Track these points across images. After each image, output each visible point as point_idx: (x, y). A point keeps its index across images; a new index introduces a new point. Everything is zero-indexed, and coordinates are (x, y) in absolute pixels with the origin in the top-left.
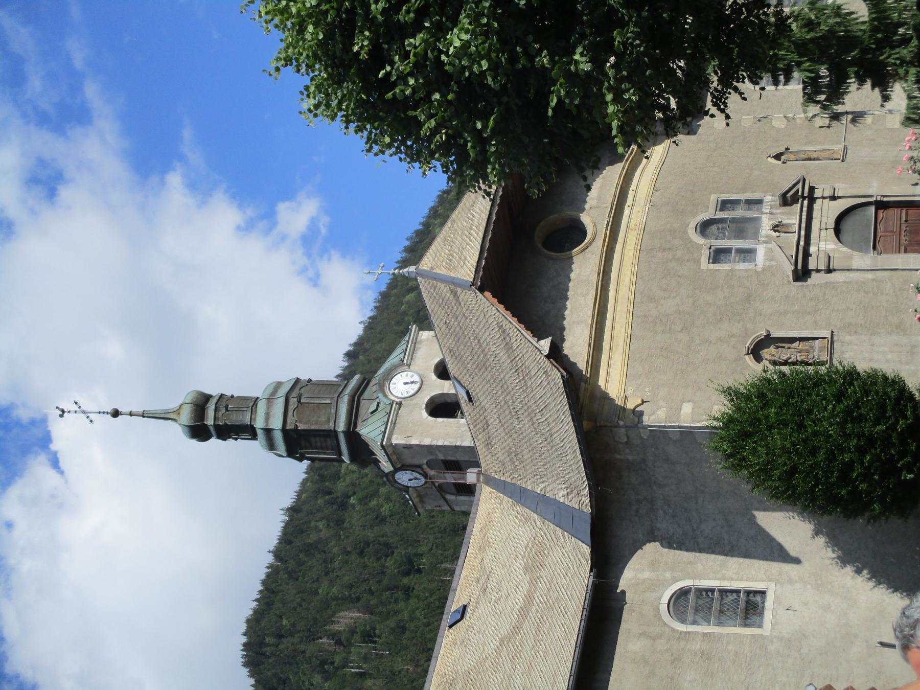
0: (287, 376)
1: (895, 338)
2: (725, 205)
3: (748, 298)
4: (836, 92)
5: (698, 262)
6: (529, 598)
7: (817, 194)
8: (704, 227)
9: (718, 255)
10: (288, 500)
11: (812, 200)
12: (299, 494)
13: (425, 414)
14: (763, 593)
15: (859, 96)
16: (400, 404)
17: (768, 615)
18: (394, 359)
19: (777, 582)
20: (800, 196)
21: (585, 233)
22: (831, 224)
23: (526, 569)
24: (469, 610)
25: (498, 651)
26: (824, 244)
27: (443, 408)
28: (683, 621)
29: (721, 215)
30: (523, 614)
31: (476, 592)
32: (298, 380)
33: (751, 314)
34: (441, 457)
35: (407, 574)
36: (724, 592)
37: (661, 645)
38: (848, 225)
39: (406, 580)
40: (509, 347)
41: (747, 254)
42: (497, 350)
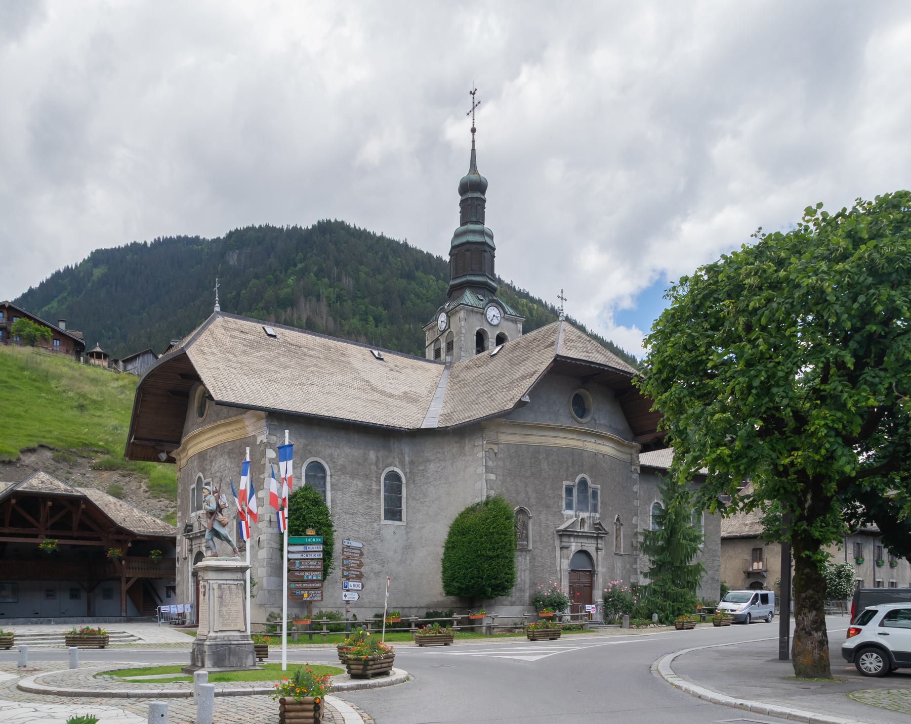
0: (497, 242)
1: (528, 581)
2: (594, 493)
3: (548, 507)
4: (646, 549)
5: (567, 480)
6: (391, 396)
7: (599, 542)
8: (583, 483)
9: (569, 491)
10: (411, 243)
11: (597, 538)
12: (415, 250)
13: (477, 329)
14: (401, 520)
15: (645, 562)
16: (482, 314)
17: (390, 522)
18: (509, 310)
19: (407, 526)
20: (599, 533)
21: (581, 417)
22: (584, 548)
23: (405, 393)
24: (381, 362)
25: (363, 380)
26: (575, 546)
27: (481, 338)
28: (385, 479)
29: (590, 491)
30: (383, 393)
31: (391, 365)
32: (494, 249)
33: (540, 509)
34: (455, 340)
35: (375, 318)
36: (400, 499)
37: (373, 468)
38: (583, 557)
39: (371, 319)
40: (524, 377)
41: (569, 506)
42: (522, 370)
